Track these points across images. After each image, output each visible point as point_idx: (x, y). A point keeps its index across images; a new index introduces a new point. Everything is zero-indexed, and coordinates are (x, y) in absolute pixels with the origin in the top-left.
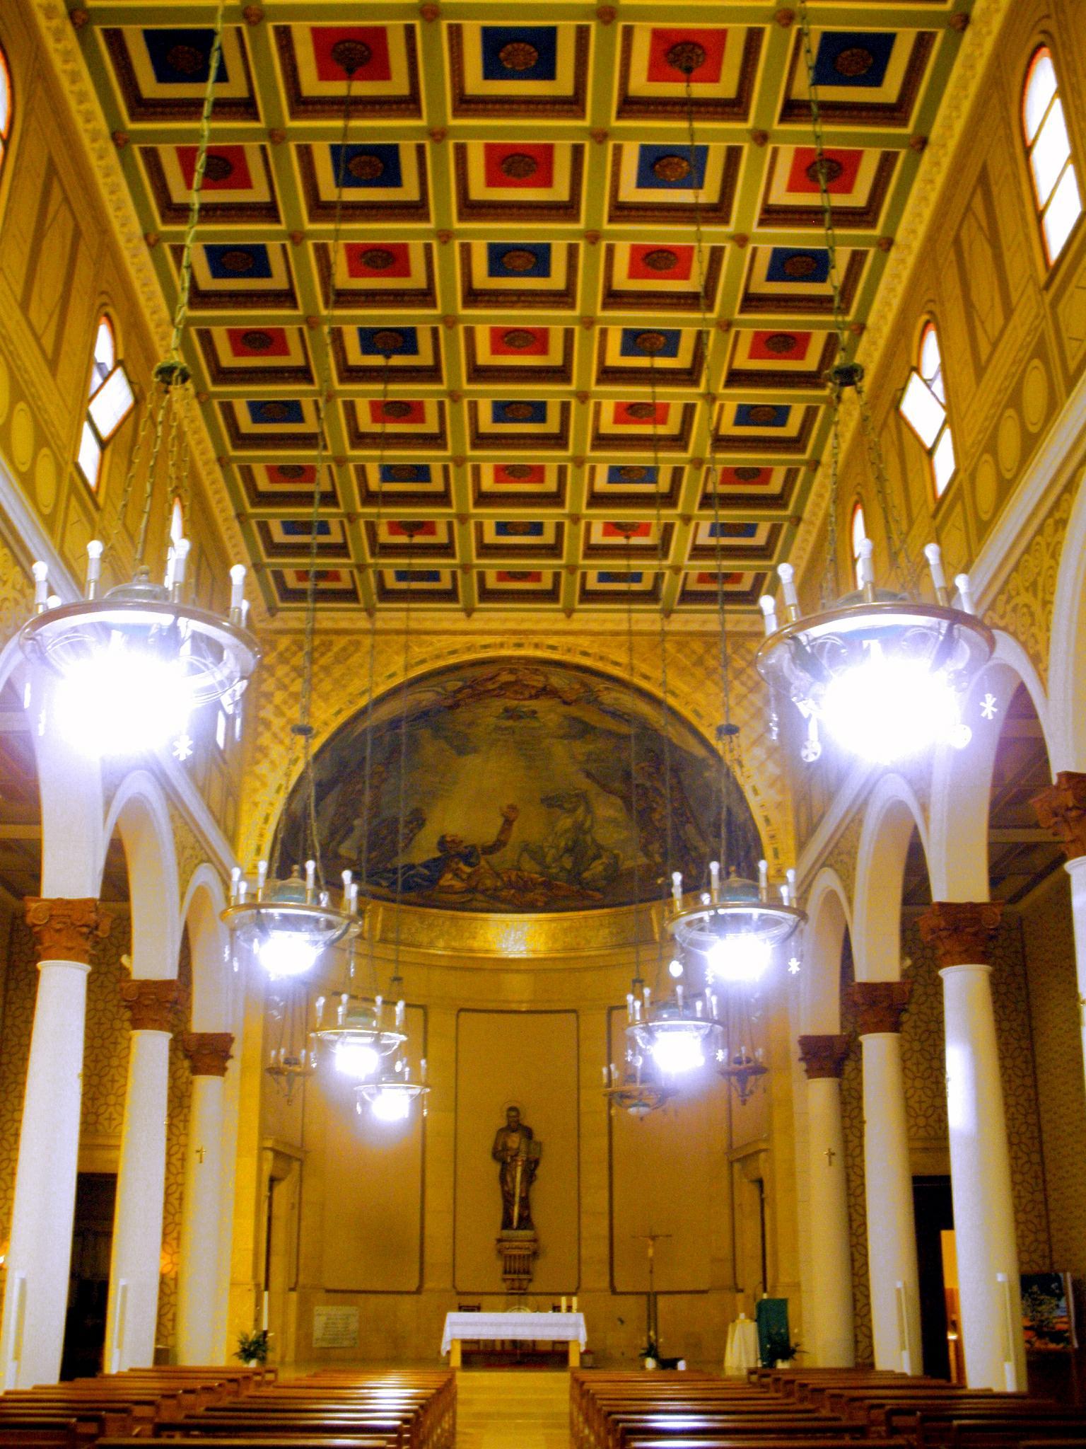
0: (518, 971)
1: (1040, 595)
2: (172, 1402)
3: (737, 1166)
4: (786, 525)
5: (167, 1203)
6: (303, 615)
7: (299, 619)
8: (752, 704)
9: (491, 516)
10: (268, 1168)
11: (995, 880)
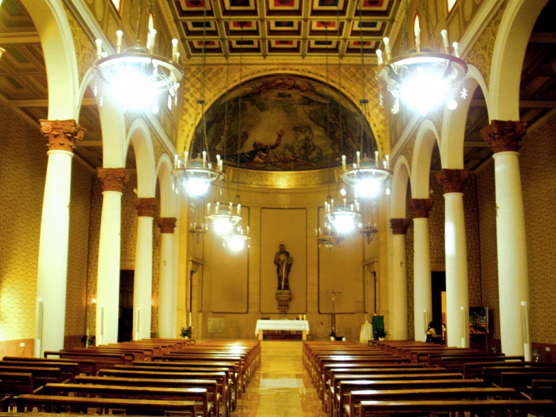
0: (284, 193)
1: (488, 50)
2: (158, 350)
3: (366, 267)
4: (388, 23)
5: (153, 281)
6: (200, 58)
7: (199, 60)
8: (374, 92)
9: (273, 19)
10: (190, 267)
11: (466, 161)
